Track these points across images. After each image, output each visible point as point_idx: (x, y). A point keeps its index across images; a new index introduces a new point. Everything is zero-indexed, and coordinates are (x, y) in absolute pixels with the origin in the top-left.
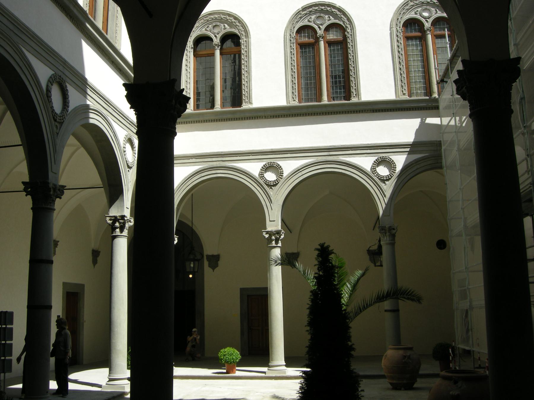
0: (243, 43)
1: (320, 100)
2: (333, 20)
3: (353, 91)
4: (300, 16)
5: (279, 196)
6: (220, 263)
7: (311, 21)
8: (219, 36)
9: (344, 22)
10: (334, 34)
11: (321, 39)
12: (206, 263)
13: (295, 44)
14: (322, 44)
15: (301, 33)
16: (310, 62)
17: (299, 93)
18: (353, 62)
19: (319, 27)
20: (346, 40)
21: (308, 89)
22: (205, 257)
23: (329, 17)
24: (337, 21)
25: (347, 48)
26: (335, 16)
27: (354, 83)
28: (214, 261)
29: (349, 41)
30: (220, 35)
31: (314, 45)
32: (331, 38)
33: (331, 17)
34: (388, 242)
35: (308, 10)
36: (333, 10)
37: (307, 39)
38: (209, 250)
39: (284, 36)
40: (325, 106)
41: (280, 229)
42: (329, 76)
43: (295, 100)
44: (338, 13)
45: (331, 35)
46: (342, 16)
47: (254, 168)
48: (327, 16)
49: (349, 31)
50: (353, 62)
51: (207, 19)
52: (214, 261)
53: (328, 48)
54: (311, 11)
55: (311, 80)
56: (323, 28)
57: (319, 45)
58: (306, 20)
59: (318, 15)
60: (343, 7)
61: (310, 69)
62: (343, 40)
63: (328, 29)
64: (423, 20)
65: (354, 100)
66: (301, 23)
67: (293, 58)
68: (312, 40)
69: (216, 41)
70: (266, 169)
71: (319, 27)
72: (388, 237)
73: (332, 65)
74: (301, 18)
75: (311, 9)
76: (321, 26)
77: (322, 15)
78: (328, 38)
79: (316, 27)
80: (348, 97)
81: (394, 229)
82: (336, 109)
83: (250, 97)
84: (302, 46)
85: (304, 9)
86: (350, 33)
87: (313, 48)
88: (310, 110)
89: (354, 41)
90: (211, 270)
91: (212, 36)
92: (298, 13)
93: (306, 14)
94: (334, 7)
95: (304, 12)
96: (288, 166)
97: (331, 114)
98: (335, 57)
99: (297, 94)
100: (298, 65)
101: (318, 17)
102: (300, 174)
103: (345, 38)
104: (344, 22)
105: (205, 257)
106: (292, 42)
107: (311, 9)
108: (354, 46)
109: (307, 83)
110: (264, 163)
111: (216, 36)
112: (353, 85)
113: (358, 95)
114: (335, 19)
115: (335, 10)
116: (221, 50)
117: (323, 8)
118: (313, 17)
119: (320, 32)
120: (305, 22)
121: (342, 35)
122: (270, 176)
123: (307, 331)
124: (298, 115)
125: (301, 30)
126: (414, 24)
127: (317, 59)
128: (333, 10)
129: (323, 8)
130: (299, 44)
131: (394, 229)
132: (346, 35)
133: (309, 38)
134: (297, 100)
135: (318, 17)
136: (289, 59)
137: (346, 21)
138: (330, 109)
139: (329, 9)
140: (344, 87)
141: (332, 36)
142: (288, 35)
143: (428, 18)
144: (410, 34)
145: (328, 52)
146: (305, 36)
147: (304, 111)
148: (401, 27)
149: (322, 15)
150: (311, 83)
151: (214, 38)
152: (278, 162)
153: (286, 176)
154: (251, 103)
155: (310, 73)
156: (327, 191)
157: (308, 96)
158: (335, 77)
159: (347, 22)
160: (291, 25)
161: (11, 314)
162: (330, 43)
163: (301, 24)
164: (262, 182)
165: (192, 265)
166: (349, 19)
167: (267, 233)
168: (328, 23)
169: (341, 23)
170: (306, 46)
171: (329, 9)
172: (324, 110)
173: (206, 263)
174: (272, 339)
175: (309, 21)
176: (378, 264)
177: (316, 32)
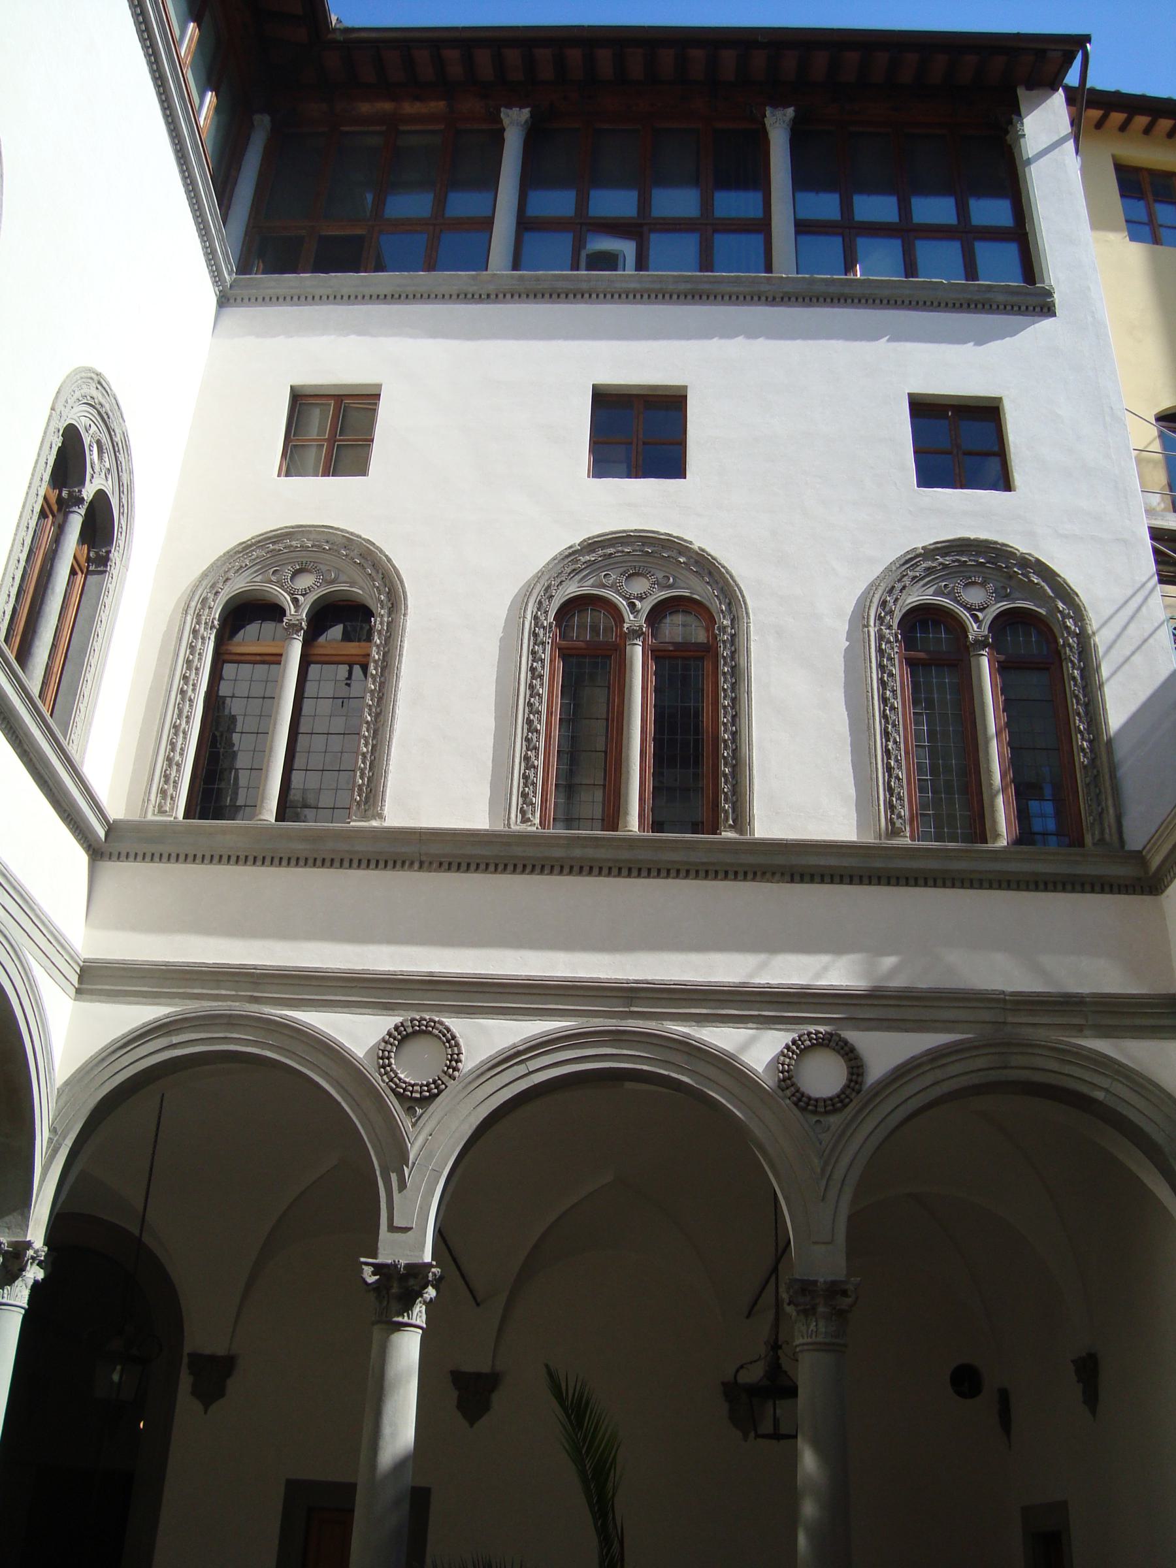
0: (379, 627)
5: (434, 1145)
6: (232, 1384)
8: (306, 603)
12: (185, 1381)
13: (548, 648)
19: (632, 606)
22: (185, 1360)
28: (214, 1375)
30: (312, 597)
34: (820, 1339)
38: (204, 1333)
40: (632, 842)
41: (427, 1257)
47: (358, 1032)
51: (276, 547)
52: (214, 1375)
56: (644, 607)
63: (657, 614)
64: (965, 615)
69: (297, 614)
70: (402, 1037)
71: (632, 606)
72: (821, 1323)
76: (301, 598)
79: (622, 604)
81: (844, 1293)
90: (197, 1406)
91: (286, 600)
96: (483, 1037)
100: (550, 713)
102: (521, 1070)
105: (185, 1360)
110: (398, 1020)
111: (295, 601)
113: (741, 820)
116: (306, 645)
122: (412, 1069)
123: (888, 341)
126: (937, 623)
131: (844, 1293)
134: (537, 821)
141: (675, 628)
143: (981, 610)
148: (895, 626)
151: (291, 609)
152: (447, 1021)
153: (471, 1072)
154: (380, 816)
156: (610, 1132)
161: (294, 1489)
163: (572, 589)
164: (379, 1082)
165: (116, 1377)
167: (378, 1269)
173: (185, 1381)
176: (767, 1427)
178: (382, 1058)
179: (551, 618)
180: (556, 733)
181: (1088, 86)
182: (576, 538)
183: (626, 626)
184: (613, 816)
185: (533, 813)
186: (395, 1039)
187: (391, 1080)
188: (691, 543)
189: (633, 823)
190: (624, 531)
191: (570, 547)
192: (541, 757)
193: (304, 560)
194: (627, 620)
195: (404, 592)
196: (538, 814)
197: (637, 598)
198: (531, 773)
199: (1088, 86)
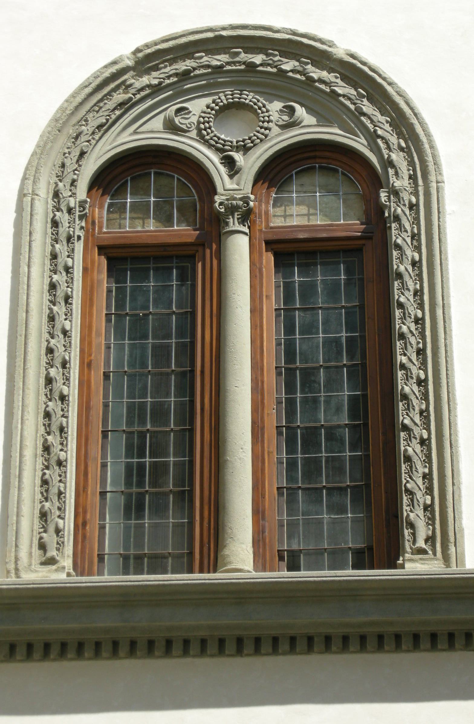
1: (213, 558)
2: (309, 127)
3: (418, 517)
4: (119, 97)
7: (185, 125)
9: (372, 138)
10: (312, 205)
11: (234, 224)
13: (79, 247)
14: (239, 249)
15: (120, 192)
16: (161, 353)
17: (81, 525)
18: (421, 352)
19: (229, 162)
20: (385, 231)
21: (140, 508)
23: (291, 111)
24: (334, 133)
25: (385, 276)
26: (326, 105)
27: (422, 470)
29: (397, 237)
31: (192, 258)
32: (295, 222)
33: (300, 111)
35: (169, 70)
36: (316, 73)
37: (152, 225)
39: (22, 195)
40: (242, 595)
42: (270, 432)
43: (52, 561)
44: (342, 88)
45: (294, 209)
46: (367, 107)
48: (276, 106)
49: (401, 183)
50: (421, 352)
53: (271, 277)
54: (185, 75)
55: (158, 450)
56: (250, 163)
57: (220, 255)
58: (158, 123)
59: (225, 96)
60: (372, 60)
61: (161, 388)
62: (366, 236)
63: (277, 172)
65: (416, 567)
66: (125, 137)
67: (61, 321)
68: (181, 231)
71: (229, 162)
73: (290, 372)
74: (125, 106)
75: (182, 66)
76: (238, 157)
77: (249, 97)
78: (277, 222)
79: (211, 159)
80: (384, 545)
82: (304, 619)
83: (442, 515)
84: (122, 259)
85: (149, 59)
86: (406, 196)
87: (187, 277)
88: (142, 620)
89: (428, 239)
92: (112, 79)
93: (156, 89)
94: (321, 57)
95: (145, 80)
97: (257, 651)
98: (309, 329)
99: (68, 524)
100: (86, 365)
101: (224, 111)
103: (377, 222)
104: (372, 138)
106: (63, 230)
107: (182, 66)
108: (429, 266)
109: (141, 467)
112: (413, 481)
113: (444, 538)
114: (324, 119)
115: (324, 74)
117: (258, 59)
118: (198, 106)
119: (229, 187)
120: (152, 132)
121: (358, 207)
124: (80, 648)
125: (119, 175)
127: (203, 334)
128: (316, 73)
129: (258, 59)
130: (102, 249)
132: (380, 209)
133: (168, 220)
134: (67, 563)
135: (224, 111)
136: (37, 322)
137: (385, 129)
138: (267, 619)
139: (288, 65)
140: (362, 495)
141: (302, 212)
142: (44, 192)
144: (277, 569)
145: (271, 303)
146: (141, 210)
147: (106, 621)
149: (249, 97)
150: (159, 471)
155: (160, 413)
157: (139, 544)
158: (311, 438)
159: (393, 139)
160: (63, 141)
162: (287, 252)
166: (403, 123)
168: (278, 140)
169: (360, 144)
170: (146, 259)
171: (288, 65)
172: (230, 619)
174: (225, 404)
175: (171, 127)
177: (205, 183)
178: (203, 123)
179: (82, 192)
180: (100, 340)
181: (316, 123)
182: (123, 44)
183: (218, 199)
184: (212, 549)
185: (60, 546)
186: (212, 109)
187: (217, 143)
188: (331, 44)
189: (241, 558)
190: (211, 30)
191: (114, 63)
192: (72, 444)
193: (71, 399)
194: (220, 189)
195: (428, 135)
196: (69, 549)
197: (238, 149)
198: (53, 474)
199: (316, 123)
